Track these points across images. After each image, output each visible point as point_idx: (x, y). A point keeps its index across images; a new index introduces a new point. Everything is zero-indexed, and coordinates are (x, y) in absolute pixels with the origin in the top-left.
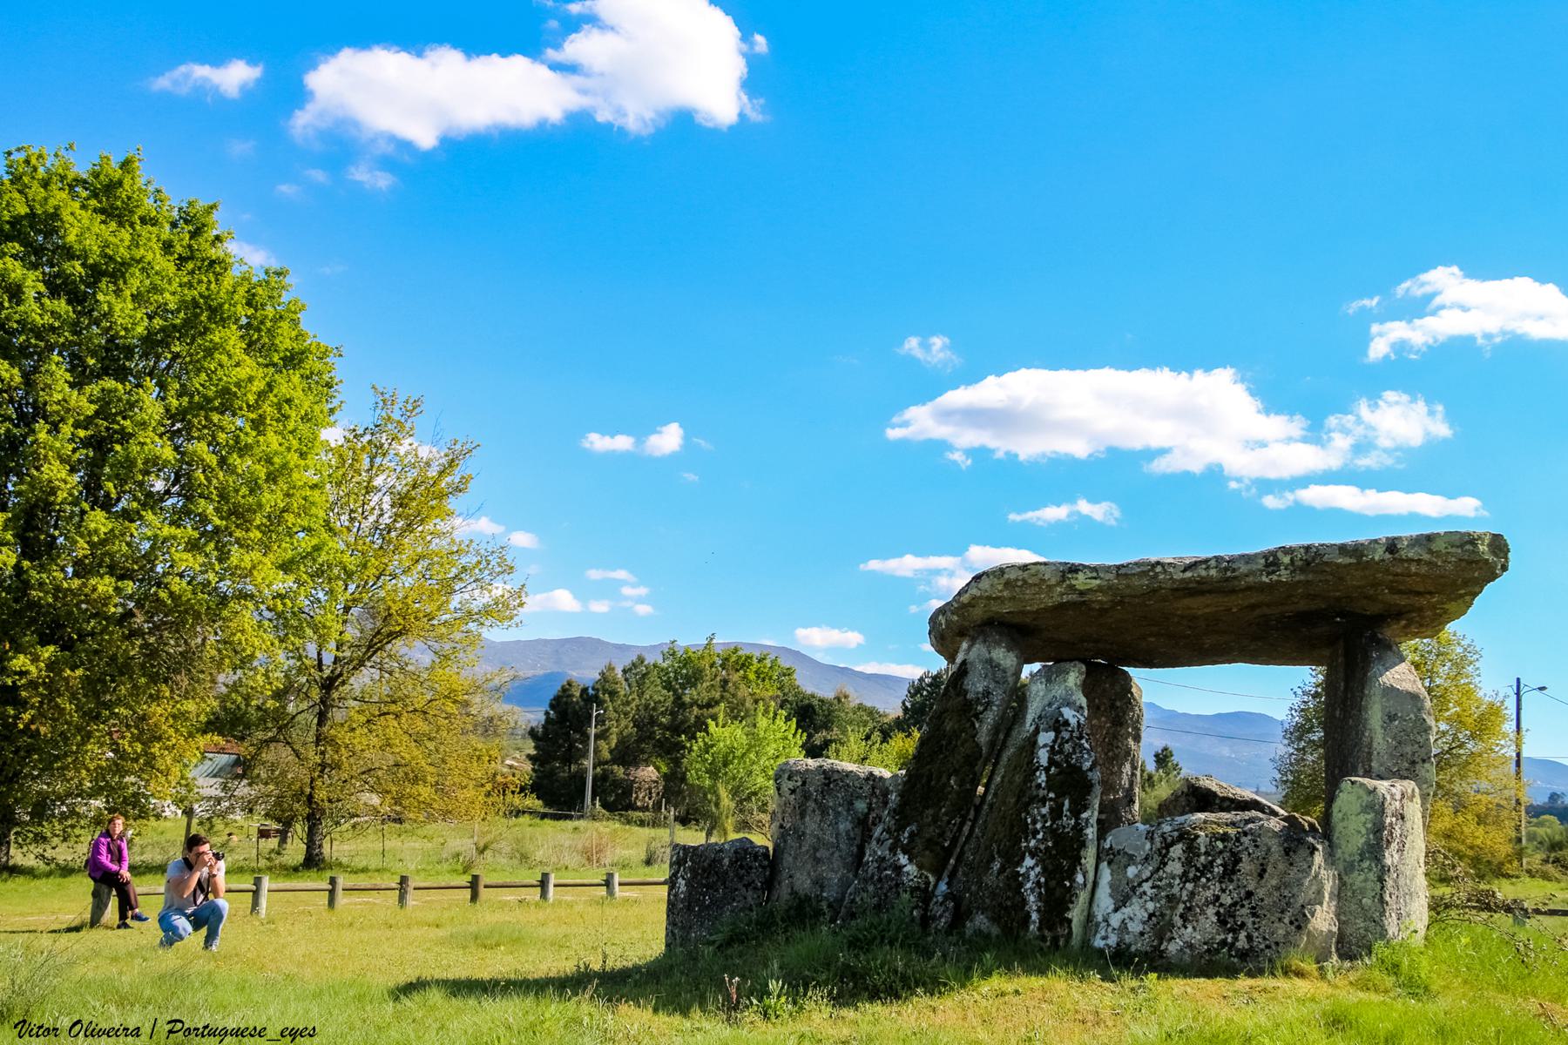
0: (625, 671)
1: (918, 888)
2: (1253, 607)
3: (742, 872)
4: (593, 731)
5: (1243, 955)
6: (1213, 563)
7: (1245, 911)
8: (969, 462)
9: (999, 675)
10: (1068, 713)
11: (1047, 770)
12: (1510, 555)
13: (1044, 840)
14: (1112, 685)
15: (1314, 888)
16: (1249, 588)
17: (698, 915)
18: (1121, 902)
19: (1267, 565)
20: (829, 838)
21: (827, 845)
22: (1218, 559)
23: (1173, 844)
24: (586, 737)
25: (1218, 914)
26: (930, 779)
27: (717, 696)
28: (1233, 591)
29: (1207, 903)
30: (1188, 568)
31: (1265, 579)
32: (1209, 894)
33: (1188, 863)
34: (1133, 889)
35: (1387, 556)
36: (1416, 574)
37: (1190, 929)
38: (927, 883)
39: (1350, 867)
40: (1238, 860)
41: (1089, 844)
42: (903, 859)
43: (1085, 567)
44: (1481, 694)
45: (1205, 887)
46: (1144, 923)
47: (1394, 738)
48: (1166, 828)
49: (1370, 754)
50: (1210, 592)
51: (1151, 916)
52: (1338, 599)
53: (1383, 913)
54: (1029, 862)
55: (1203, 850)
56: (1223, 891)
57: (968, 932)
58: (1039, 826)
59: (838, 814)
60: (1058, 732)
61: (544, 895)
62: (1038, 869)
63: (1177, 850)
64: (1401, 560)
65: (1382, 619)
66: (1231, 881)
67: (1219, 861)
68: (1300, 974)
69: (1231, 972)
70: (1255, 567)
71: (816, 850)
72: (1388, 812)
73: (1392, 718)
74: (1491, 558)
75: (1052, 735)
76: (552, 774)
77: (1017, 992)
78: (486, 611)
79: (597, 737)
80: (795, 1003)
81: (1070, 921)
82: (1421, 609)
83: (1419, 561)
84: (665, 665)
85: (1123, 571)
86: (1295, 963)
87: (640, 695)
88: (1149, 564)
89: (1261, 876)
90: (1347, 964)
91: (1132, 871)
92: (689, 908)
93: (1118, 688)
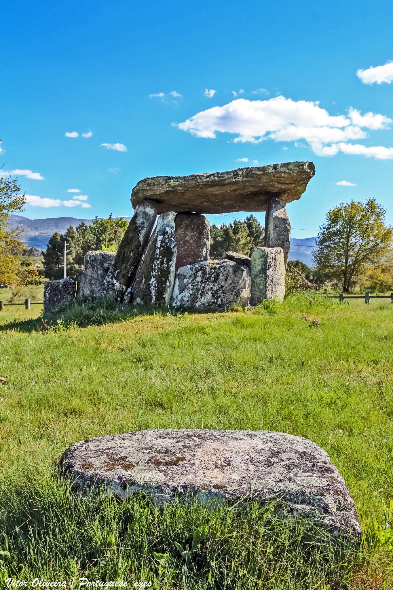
0: (77, 229)
1: (120, 291)
2: (235, 190)
3: (66, 289)
4: (65, 252)
5: (220, 306)
6: (216, 175)
7: (221, 292)
9: (147, 217)
10: (168, 229)
11: (160, 248)
12: (315, 169)
13: (158, 272)
14: (198, 221)
15: (243, 283)
16: (229, 184)
17: (53, 305)
18: (182, 290)
19: (234, 175)
20: (95, 276)
21: (95, 279)
22: (218, 173)
23: (199, 271)
24: (63, 254)
25: (212, 293)
26: (124, 254)
27: (113, 237)
28: (224, 185)
29: (209, 290)
30: (208, 177)
31: (234, 180)
32: (209, 287)
33: (203, 277)
34: (186, 287)
35: (273, 171)
36: (284, 177)
37: (203, 298)
38: (123, 289)
39: (256, 276)
40: (219, 275)
41: (171, 272)
42: (115, 281)
43: (173, 177)
44: (385, 226)
45: (208, 285)
46: (189, 297)
47: (277, 234)
48: (197, 266)
49: (269, 239)
50: (217, 185)
51: (191, 295)
52: (262, 187)
53: (266, 291)
54: (153, 279)
55: (208, 272)
56: (214, 286)
57: (135, 304)
58: (156, 267)
59: (98, 268)
60: (164, 236)
61: (27, 307)
62: (155, 282)
63: (200, 273)
64: (279, 172)
65: (279, 194)
66: (216, 282)
67: (213, 276)
68: (237, 311)
69: (214, 311)
70: (230, 176)
71: (91, 280)
72: (269, 257)
73: (276, 227)
74: (308, 170)
75: (162, 236)
76: (51, 268)
77: (142, 321)
78: (10, 206)
79: (67, 254)
80: (66, 327)
81: (164, 298)
82: (290, 190)
83: (284, 172)
84: (94, 226)
85: (186, 179)
86: (236, 307)
87: (84, 238)
88: (195, 176)
89: (226, 280)
90: (253, 307)
91: (185, 281)
92: (50, 303)
93: (200, 222)
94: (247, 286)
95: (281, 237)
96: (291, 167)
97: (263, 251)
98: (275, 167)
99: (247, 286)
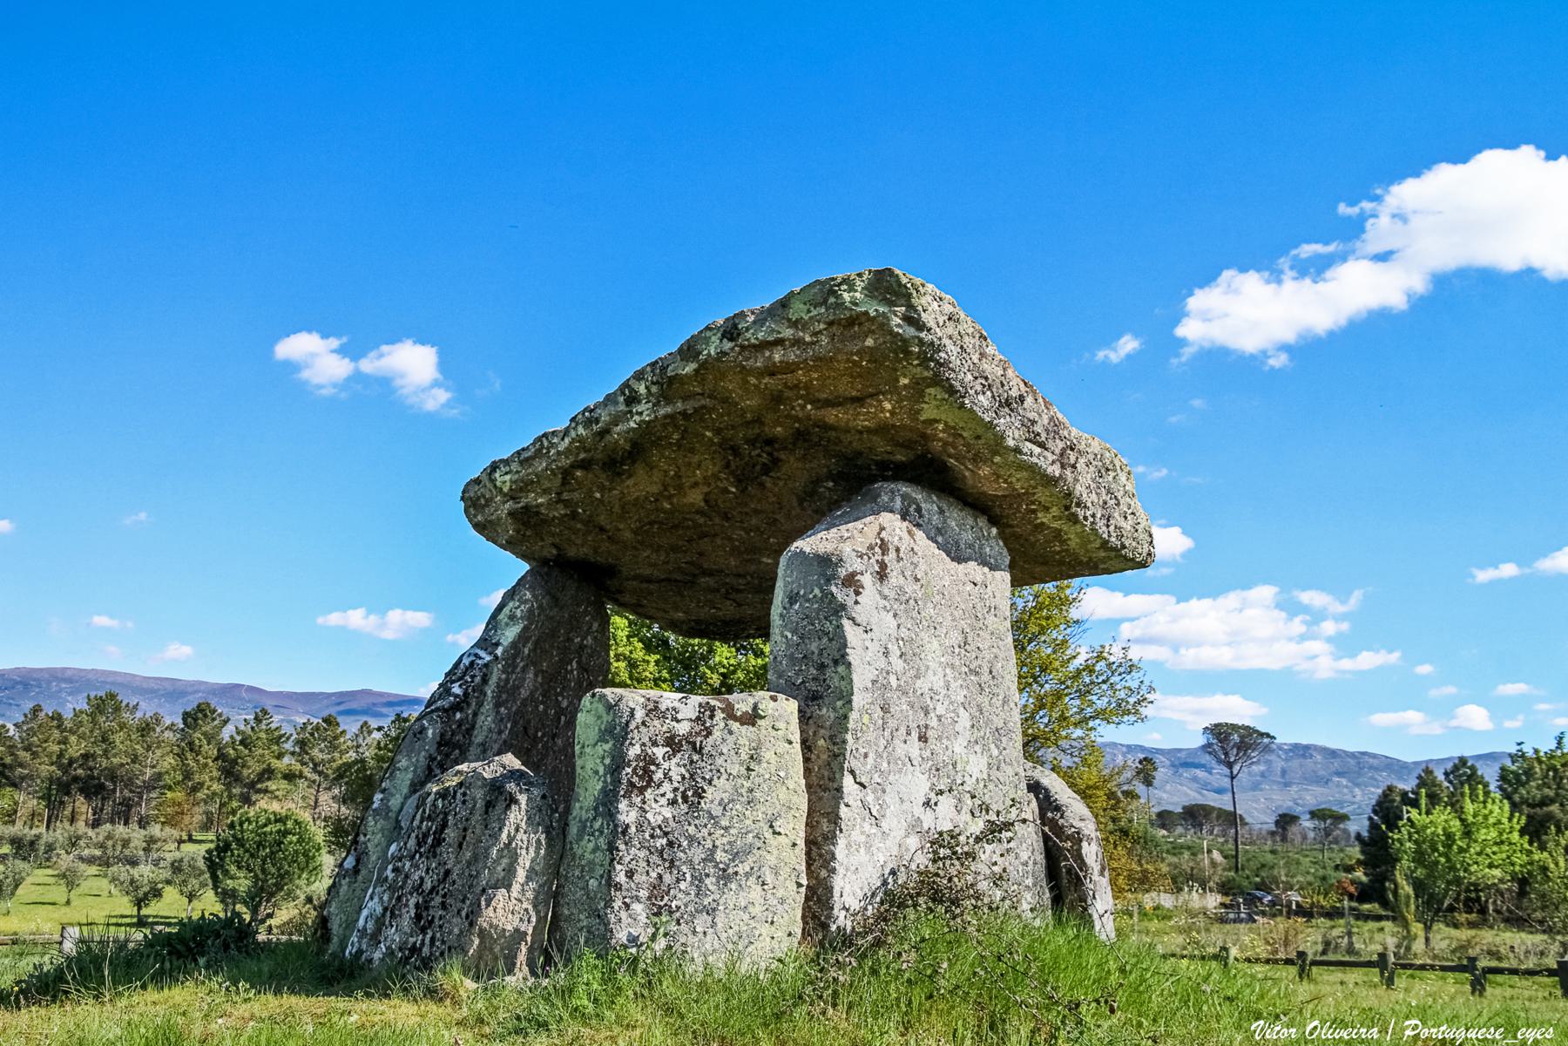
0: (1446, 774)
8: (442, 396)
35: (727, 345)
47: (794, 632)
94: (521, 875)
95: (814, 647)
96: (798, 310)
97: (610, 707)
98: (731, 331)
99: (521, 875)
